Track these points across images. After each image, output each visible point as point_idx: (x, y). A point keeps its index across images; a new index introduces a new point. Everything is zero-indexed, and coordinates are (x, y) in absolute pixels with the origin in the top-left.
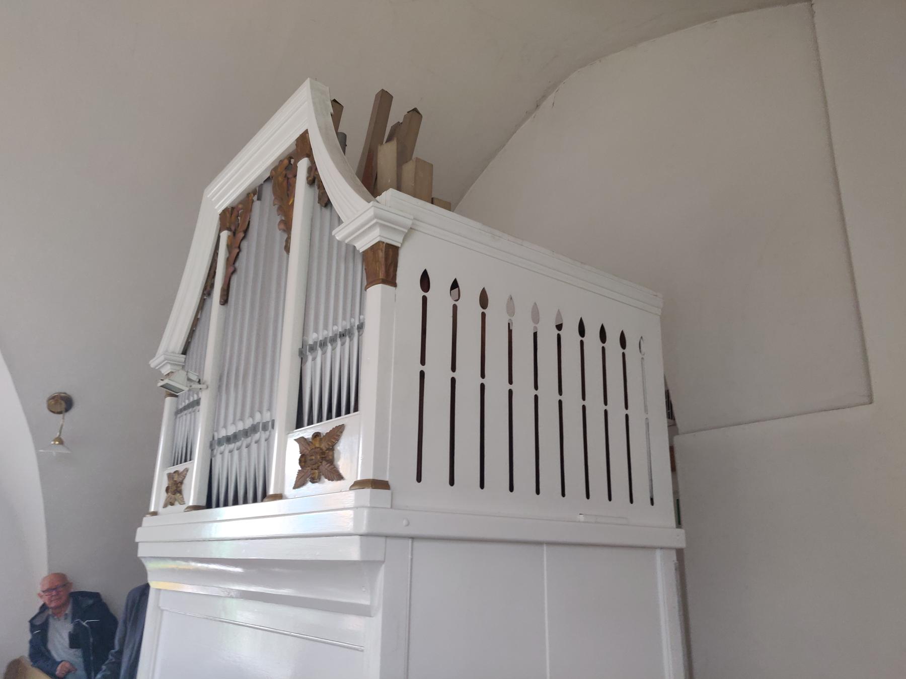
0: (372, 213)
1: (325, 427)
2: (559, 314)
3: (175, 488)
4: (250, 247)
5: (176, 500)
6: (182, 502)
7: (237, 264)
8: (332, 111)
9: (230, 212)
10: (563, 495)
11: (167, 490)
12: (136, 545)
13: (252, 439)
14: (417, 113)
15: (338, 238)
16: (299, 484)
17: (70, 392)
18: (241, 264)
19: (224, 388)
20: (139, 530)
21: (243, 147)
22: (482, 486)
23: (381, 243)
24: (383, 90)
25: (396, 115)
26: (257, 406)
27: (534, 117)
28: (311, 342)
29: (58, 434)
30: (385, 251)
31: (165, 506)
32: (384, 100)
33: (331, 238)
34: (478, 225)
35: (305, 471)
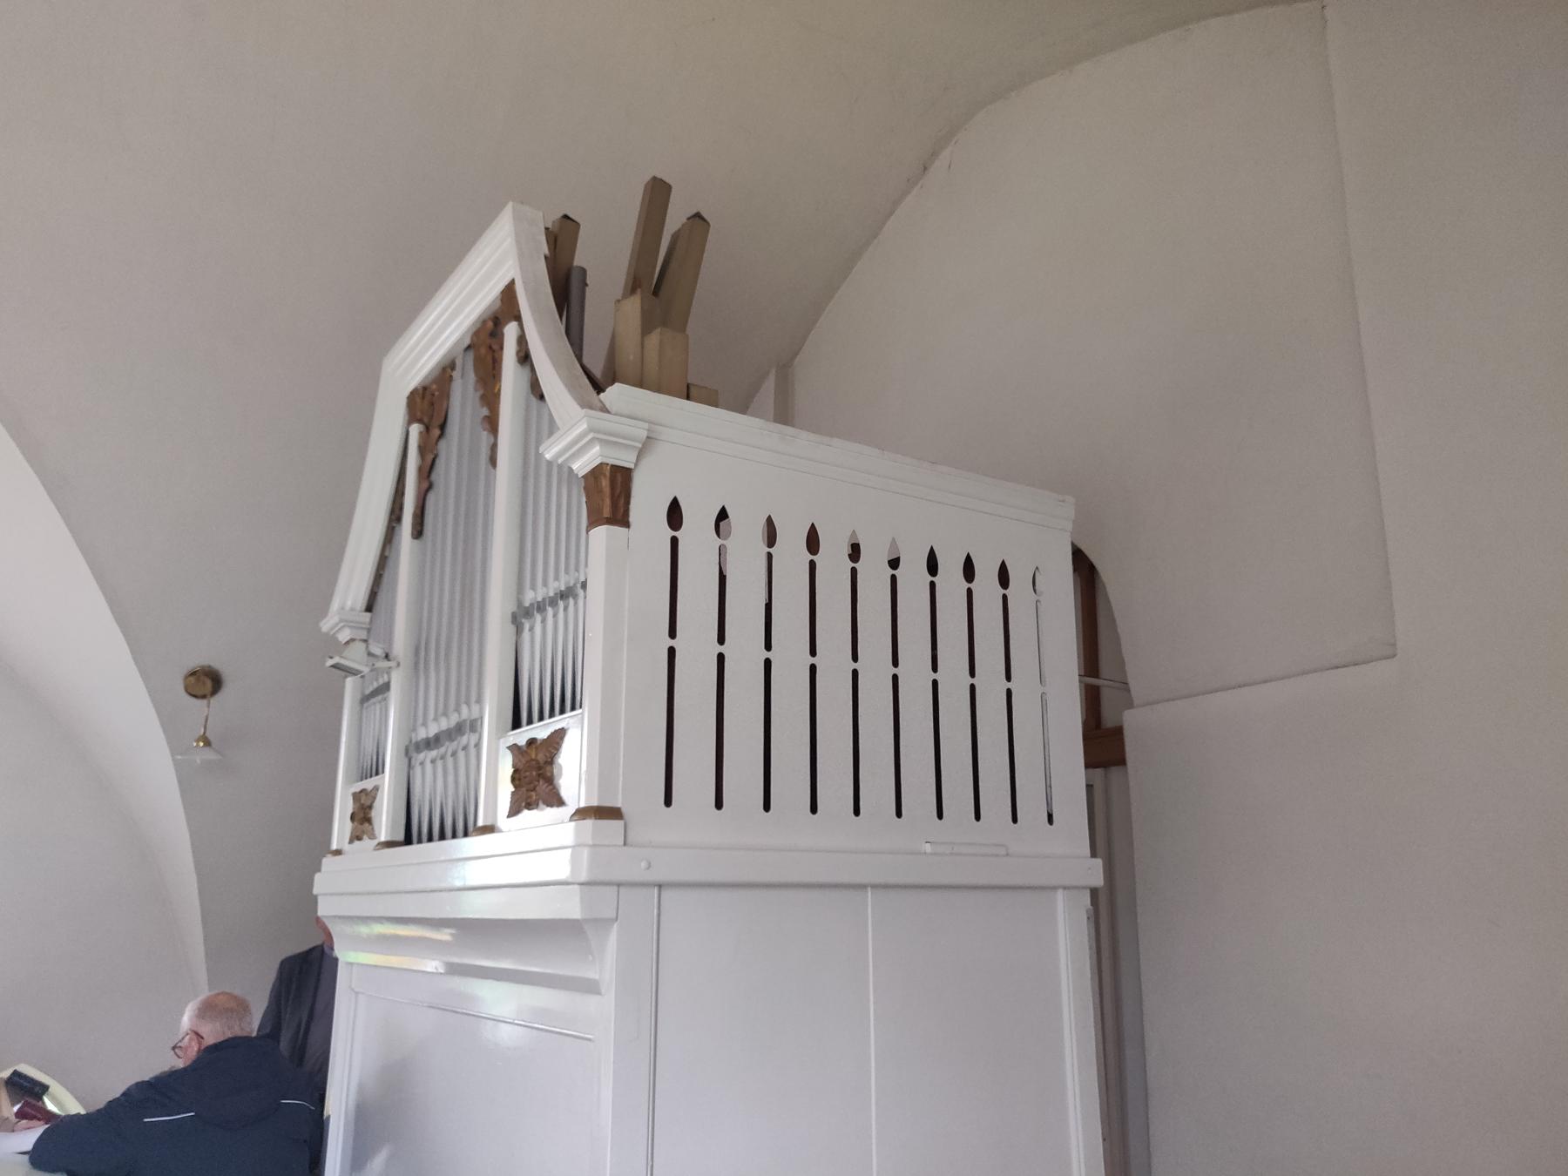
0: (585, 426)
1: (541, 731)
2: (894, 544)
3: (362, 816)
4: (450, 450)
5: (363, 832)
6: (372, 836)
7: (434, 477)
8: (547, 252)
9: (421, 396)
10: (899, 814)
11: (353, 818)
12: (314, 900)
13: (459, 743)
14: (701, 221)
15: (548, 456)
16: (514, 811)
17: (216, 664)
18: (438, 476)
19: (422, 666)
20: (317, 877)
21: (436, 290)
22: (767, 807)
23: (604, 466)
24: (655, 178)
25: (675, 220)
26: (463, 699)
27: (922, 187)
28: (527, 604)
29: (202, 730)
30: (610, 478)
31: (351, 842)
32: (658, 192)
33: (539, 456)
34: (762, 421)
35: (520, 793)
